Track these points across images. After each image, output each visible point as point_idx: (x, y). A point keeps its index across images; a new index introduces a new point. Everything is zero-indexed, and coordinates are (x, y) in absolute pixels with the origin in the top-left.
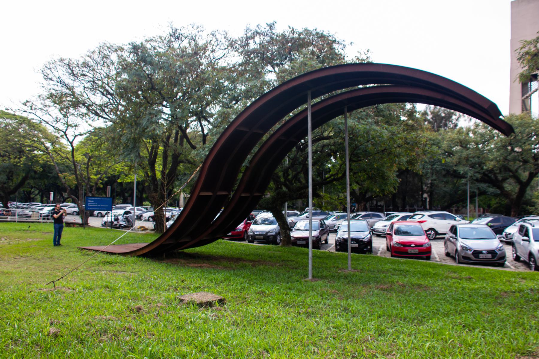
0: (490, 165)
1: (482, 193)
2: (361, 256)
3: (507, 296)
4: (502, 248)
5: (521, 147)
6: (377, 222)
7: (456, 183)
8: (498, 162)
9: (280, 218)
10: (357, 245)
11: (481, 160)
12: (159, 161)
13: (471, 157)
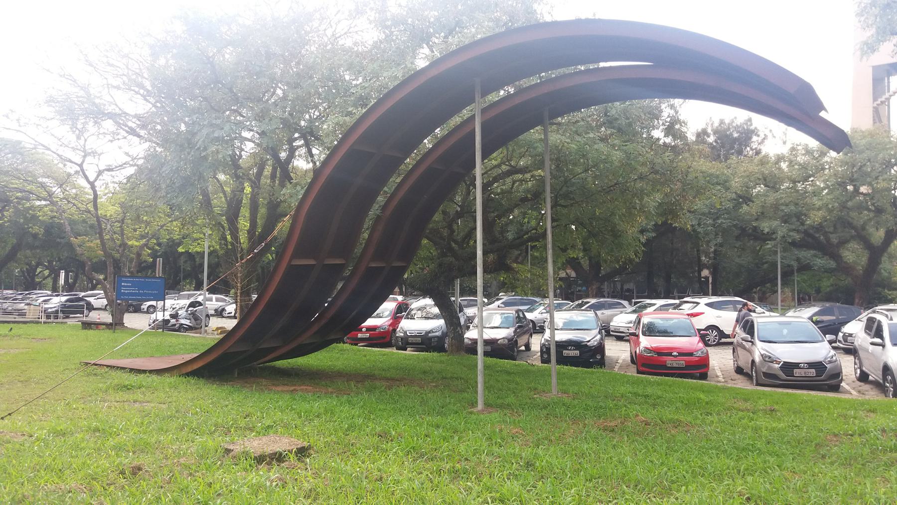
0: (815, 218)
1: (804, 268)
2: (582, 371)
3: (837, 443)
4: (834, 358)
5: (870, 184)
6: (616, 315)
7: (759, 251)
8: (830, 211)
9: (449, 312)
10: (577, 353)
11: (800, 209)
12: (245, 212)
13: (782, 204)
